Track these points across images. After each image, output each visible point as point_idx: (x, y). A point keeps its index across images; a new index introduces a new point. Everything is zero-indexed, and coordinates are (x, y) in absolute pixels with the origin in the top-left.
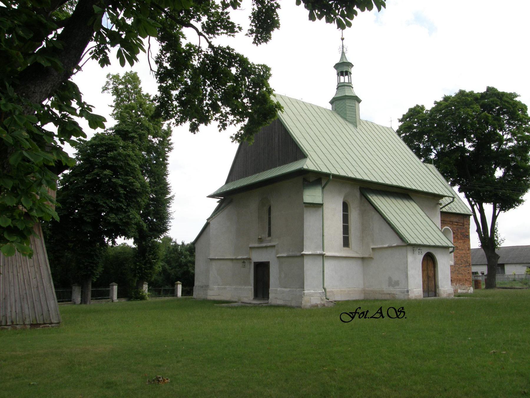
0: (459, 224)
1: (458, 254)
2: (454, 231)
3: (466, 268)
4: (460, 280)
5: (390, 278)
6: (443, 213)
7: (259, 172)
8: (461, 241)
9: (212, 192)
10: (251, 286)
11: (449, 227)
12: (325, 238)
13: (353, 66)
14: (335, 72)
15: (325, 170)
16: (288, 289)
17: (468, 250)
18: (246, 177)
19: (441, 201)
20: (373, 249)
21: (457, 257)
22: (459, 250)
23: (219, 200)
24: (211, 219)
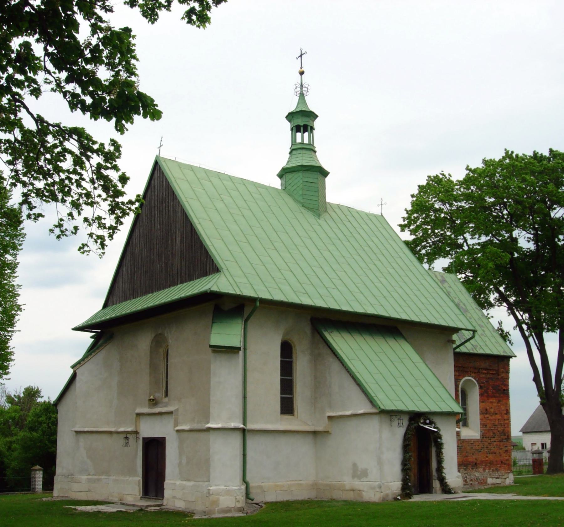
0: (491, 372)
1: (488, 422)
2: (483, 383)
3: (502, 443)
5: (355, 465)
6: (459, 357)
7: (152, 292)
8: (494, 400)
9: (80, 322)
10: (138, 476)
11: (472, 377)
12: (248, 400)
13: (317, 116)
14: (287, 126)
15: (248, 292)
16: (191, 483)
18: (133, 298)
19: (455, 337)
20: (330, 418)
21: (486, 426)
22: (490, 414)
23: (93, 334)
24: (78, 366)
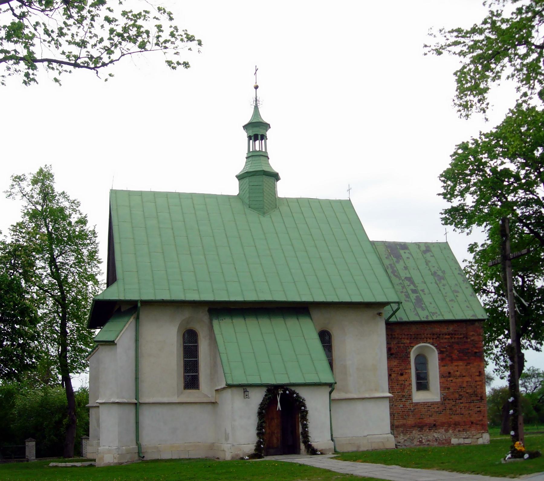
4: (456, 424)
11: (429, 343)
13: (114, 194)
14: (244, 135)
17: (479, 376)
